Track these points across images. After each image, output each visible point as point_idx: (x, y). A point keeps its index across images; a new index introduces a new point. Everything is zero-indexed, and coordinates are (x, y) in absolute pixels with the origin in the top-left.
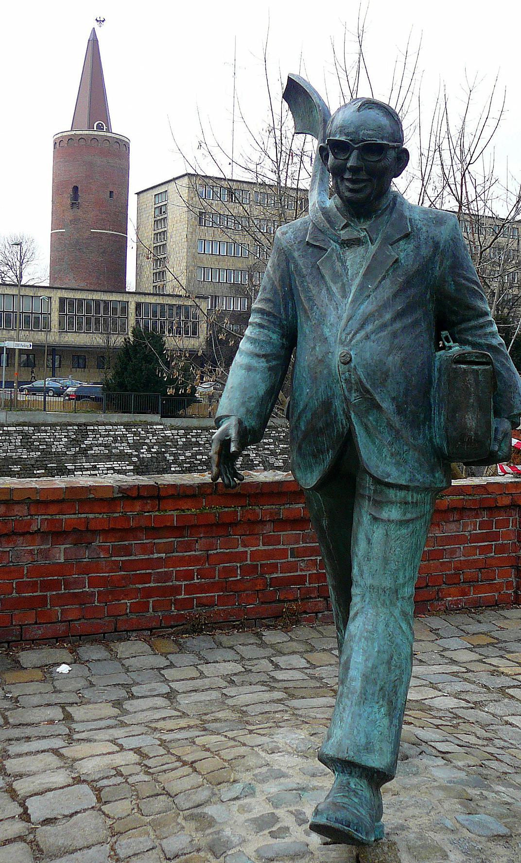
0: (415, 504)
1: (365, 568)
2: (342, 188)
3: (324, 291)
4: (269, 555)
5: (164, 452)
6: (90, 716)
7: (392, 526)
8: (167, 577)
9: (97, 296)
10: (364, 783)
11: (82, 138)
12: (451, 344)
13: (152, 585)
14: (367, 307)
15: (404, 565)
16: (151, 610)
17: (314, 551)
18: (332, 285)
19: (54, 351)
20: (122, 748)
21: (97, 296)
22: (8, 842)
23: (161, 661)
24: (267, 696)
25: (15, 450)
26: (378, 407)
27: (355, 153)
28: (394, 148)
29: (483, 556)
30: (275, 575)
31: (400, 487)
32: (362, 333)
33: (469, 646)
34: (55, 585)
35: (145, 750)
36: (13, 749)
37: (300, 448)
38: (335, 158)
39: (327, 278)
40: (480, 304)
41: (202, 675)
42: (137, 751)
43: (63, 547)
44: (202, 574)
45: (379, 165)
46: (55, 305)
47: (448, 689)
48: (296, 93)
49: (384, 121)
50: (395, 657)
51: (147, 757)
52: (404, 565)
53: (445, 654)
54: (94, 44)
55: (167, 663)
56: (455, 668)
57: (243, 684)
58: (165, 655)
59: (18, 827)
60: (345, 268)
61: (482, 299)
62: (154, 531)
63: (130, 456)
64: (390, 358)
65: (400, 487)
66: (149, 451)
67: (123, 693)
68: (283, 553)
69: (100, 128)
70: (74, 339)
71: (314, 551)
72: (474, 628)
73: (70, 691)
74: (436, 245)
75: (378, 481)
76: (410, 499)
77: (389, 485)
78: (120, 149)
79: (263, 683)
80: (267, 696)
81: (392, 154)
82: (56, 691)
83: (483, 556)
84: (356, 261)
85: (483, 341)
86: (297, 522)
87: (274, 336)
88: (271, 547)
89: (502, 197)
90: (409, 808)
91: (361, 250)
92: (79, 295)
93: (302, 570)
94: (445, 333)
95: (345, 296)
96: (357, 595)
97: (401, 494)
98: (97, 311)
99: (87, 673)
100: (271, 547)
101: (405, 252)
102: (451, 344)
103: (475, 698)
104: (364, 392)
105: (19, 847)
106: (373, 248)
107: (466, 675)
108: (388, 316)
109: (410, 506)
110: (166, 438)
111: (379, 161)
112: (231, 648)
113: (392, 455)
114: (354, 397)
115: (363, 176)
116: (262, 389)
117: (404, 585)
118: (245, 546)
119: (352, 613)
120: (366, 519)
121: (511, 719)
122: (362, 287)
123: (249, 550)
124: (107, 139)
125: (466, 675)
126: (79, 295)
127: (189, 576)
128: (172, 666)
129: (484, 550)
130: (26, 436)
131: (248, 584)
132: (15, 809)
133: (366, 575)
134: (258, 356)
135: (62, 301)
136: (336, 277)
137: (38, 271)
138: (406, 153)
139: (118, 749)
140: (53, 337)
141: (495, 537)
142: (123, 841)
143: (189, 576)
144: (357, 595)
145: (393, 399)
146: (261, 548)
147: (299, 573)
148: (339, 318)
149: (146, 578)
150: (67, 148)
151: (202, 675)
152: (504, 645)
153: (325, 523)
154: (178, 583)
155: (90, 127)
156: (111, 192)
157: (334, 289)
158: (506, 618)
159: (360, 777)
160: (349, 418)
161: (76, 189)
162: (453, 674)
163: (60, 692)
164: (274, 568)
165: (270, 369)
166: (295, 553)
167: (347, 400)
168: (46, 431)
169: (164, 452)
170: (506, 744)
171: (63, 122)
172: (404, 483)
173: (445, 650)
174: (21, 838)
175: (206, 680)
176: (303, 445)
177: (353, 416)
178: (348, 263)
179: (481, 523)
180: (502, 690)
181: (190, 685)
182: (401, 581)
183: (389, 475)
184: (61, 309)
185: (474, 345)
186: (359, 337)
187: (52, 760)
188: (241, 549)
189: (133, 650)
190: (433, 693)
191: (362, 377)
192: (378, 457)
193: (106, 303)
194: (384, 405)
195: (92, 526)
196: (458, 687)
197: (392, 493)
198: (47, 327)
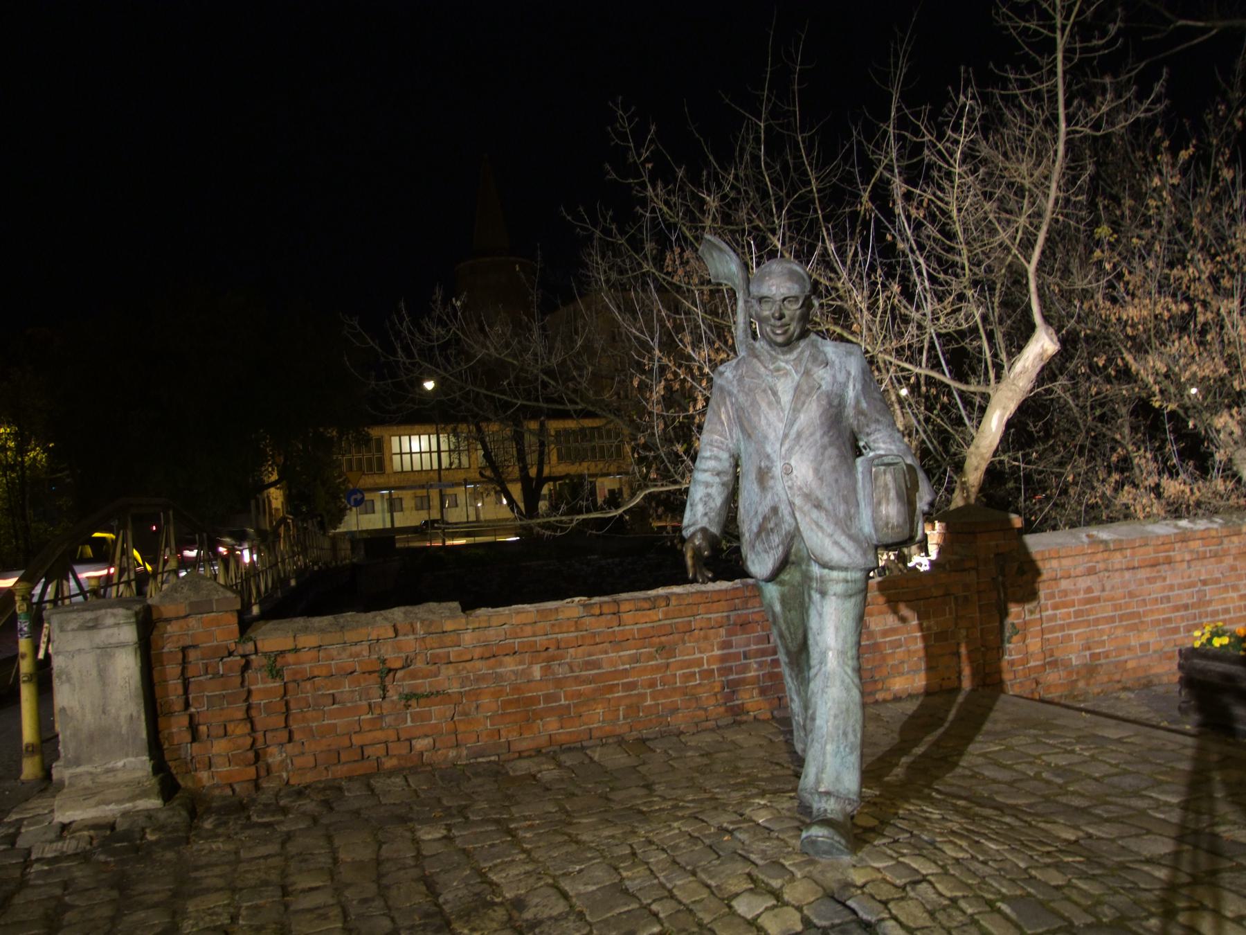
30: (731, 677)
118: (700, 652)
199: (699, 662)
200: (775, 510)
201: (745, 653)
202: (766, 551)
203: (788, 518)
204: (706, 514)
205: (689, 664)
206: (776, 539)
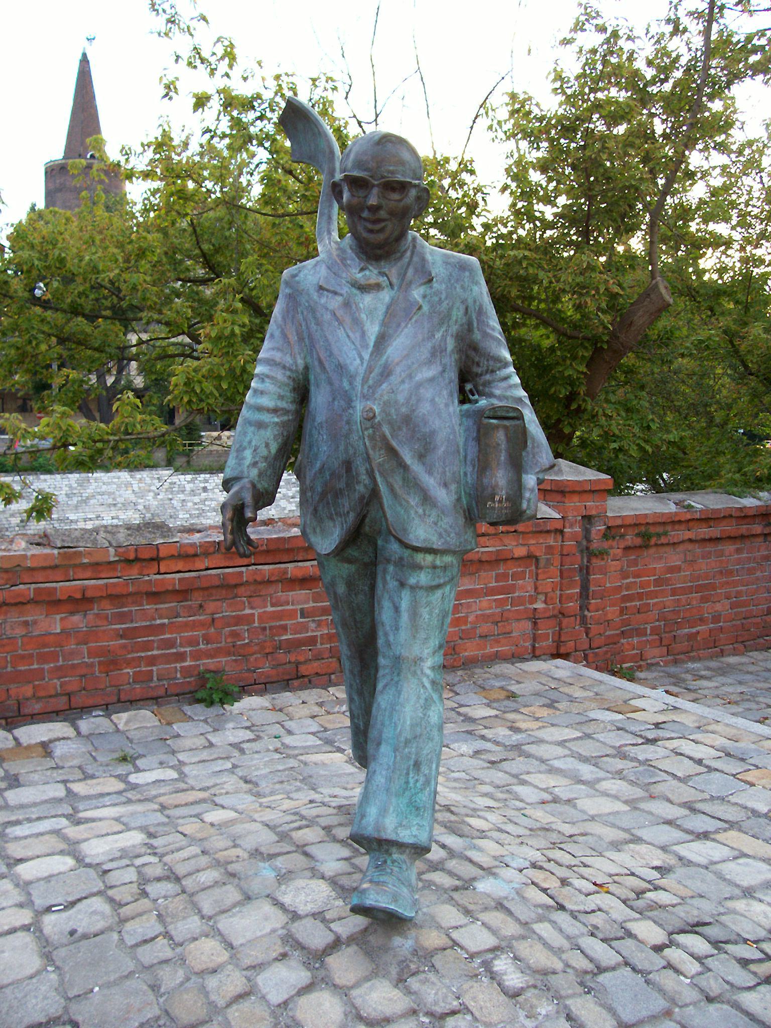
0: (445, 568)
2: (360, 228)
4: (280, 616)
8: (170, 644)
12: (476, 397)
13: (155, 652)
16: (155, 679)
17: (325, 611)
22: (13, 931)
27: (375, 191)
28: (415, 186)
29: (499, 610)
30: (284, 637)
34: (54, 657)
37: (316, 510)
38: (353, 196)
42: (143, 829)
44: (207, 640)
45: (402, 204)
53: (462, 710)
59: (25, 916)
62: (155, 596)
68: (291, 614)
71: (325, 611)
73: (71, 767)
76: (438, 563)
83: (499, 610)
86: (305, 581)
88: (279, 608)
93: (313, 631)
96: (384, 667)
97: (429, 558)
99: (90, 748)
100: (279, 608)
102: (476, 397)
105: (23, 938)
109: (438, 570)
111: (400, 200)
118: (252, 608)
119: (380, 686)
120: (392, 584)
123: (255, 612)
127: (193, 642)
129: (500, 603)
131: (256, 648)
132: (16, 896)
142: (129, 926)
143: (193, 642)
144: (384, 667)
146: (270, 609)
147: (309, 634)
149: (147, 646)
154: (182, 650)
164: (284, 628)
166: (304, 614)
171: (56, 151)
173: (461, 706)
174: (26, 928)
176: (320, 508)
179: (497, 575)
187: (53, 842)
188: (248, 611)
189: (137, 722)
195: (89, 594)
199: (249, 619)
200: (348, 465)
201: (302, 610)
202: (331, 518)
203: (364, 477)
204: (255, 464)
205: (239, 620)
206: (346, 504)
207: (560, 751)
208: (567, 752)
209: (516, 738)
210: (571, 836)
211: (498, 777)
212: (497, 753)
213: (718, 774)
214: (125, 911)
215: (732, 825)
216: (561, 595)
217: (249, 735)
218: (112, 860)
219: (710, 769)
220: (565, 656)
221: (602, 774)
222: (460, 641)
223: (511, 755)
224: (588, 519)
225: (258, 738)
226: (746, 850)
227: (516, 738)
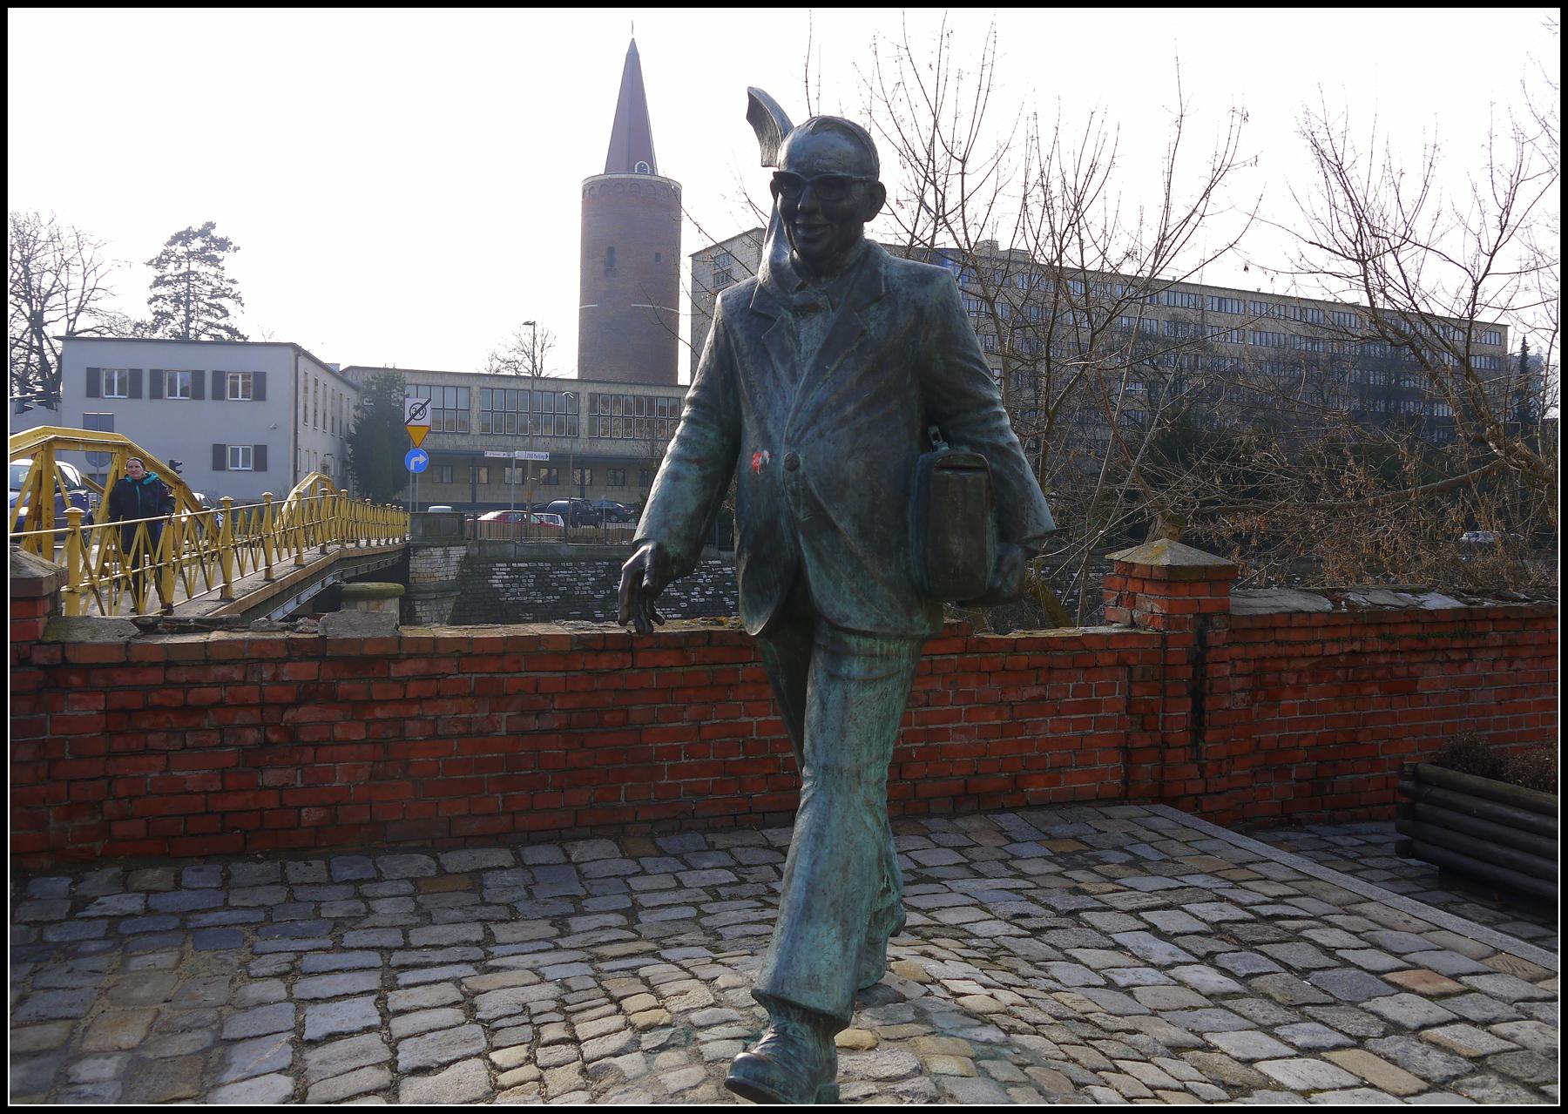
0: (886, 657)
1: (819, 742)
3: (769, 374)
5: (722, 596)
6: (518, 937)
7: (853, 686)
9: (639, 391)
10: (806, 1029)
11: (619, 183)
14: (817, 395)
15: (869, 739)
18: (777, 364)
19: (582, 462)
20: (543, 980)
21: (639, 391)
23: (629, 866)
24: (755, 916)
25: (527, 593)
26: (835, 528)
29: (1078, 733)
31: (865, 634)
32: (814, 431)
33: (1049, 853)
35: (571, 982)
36: (407, 977)
39: (773, 357)
40: (985, 391)
41: (680, 886)
43: (505, 715)
46: (584, 404)
47: (1001, 910)
48: (761, 113)
49: (848, 147)
50: (853, 861)
51: (569, 990)
52: (869, 739)
53: (1015, 864)
54: (633, 59)
55: (638, 869)
56: (1020, 883)
57: (731, 898)
58: (636, 859)
60: (799, 344)
61: (987, 383)
63: (679, 600)
64: (851, 463)
65: (865, 634)
66: (702, 594)
67: (569, 908)
69: (642, 170)
70: (605, 447)
72: (1062, 829)
74: (920, 311)
75: (835, 627)
77: (849, 632)
78: (666, 198)
79: (758, 898)
80: (755, 916)
81: (859, 190)
82: (484, 903)
83: (1078, 733)
84: (811, 334)
85: (986, 440)
87: (712, 435)
89: (1526, 240)
90: (868, 1059)
91: (818, 320)
92: (615, 390)
94: (933, 430)
95: (794, 381)
97: (866, 643)
98: (640, 410)
101: (875, 322)
103: (1033, 923)
104: (817, 510)
106: (833, 315)
107: (1031, 893)
108: (850, 409)
110: (724, 575)
112: (727, 850)
113: (853, 591)
114: (802, 515)
115: (820, 219)
116: (692, 504)
117: (868, 766)
118: (750, 715)
121: (1076, 953)
122: (818, 369)
124: (650, 184)
125: (1031, 893)
126: (615, 390)
128: (643, 873)
129: (1077, 724)
130: (541, 576)
133: (819, 751)
134: (690, 461)
135: (593, 398)
136: (786, 355)
137: (563, 361)
138: (882, 187)
139: (537, 979)
140: (581, 446)
141: (1093, 706)
145: (854, 517)
148: (787, 410)
150: (598, 195)
151: (680, 886)
152: (1097, 853)
153: (782, 681)
155: (630, 169)
156: (658, 255)
157: (782, 371)
158: (1107, 817)
159: (801, 1021)
160: (796, 541)
161: (611, 250)
162: (1017, 891)
163: (490, 904)
165: (704, 478)
167: (792, 518)
168: (567, 569)
169: (722, 596)
170: (1058, 986)
171: (596, 164)
172: (868, 629)
173: (1014, 857)
175: (684, 893)
177: (801, 539)
178: (802, 337)
180: (1073, 913)
181: (665, 898)
182: (865, 760)
183: (848, 618)
184: (592, 408)
185: (975, 446)
186: (809, 434)
189: (598, 855)
190: (978, 914)
191: (813, 486)
192: (836, 596)
193: (651, 400)
194: (842, 525)
196: (1016, 908)
197: (852, 641)
198: (573, 432)
207: (1132, 922)
208: (1142, 925)
209: (1074, 902)
210: (1035, 1024)
211: (1037, 947)
212: (1041, 918)
213: (1354, 971)
214: (504, 1079)
215: (1360, 1042)
216: (1164, 718)
217: (730, 877)
218: (510, 1016)
219: (1346, 964)
220: (1174, 802)
221: (1182, 957)
222: (1023, 772)
223: (1063, 922)
224: (1205, 618)
225: (743, 881)
226: (1371, 1079)
227: (1074, 902)
